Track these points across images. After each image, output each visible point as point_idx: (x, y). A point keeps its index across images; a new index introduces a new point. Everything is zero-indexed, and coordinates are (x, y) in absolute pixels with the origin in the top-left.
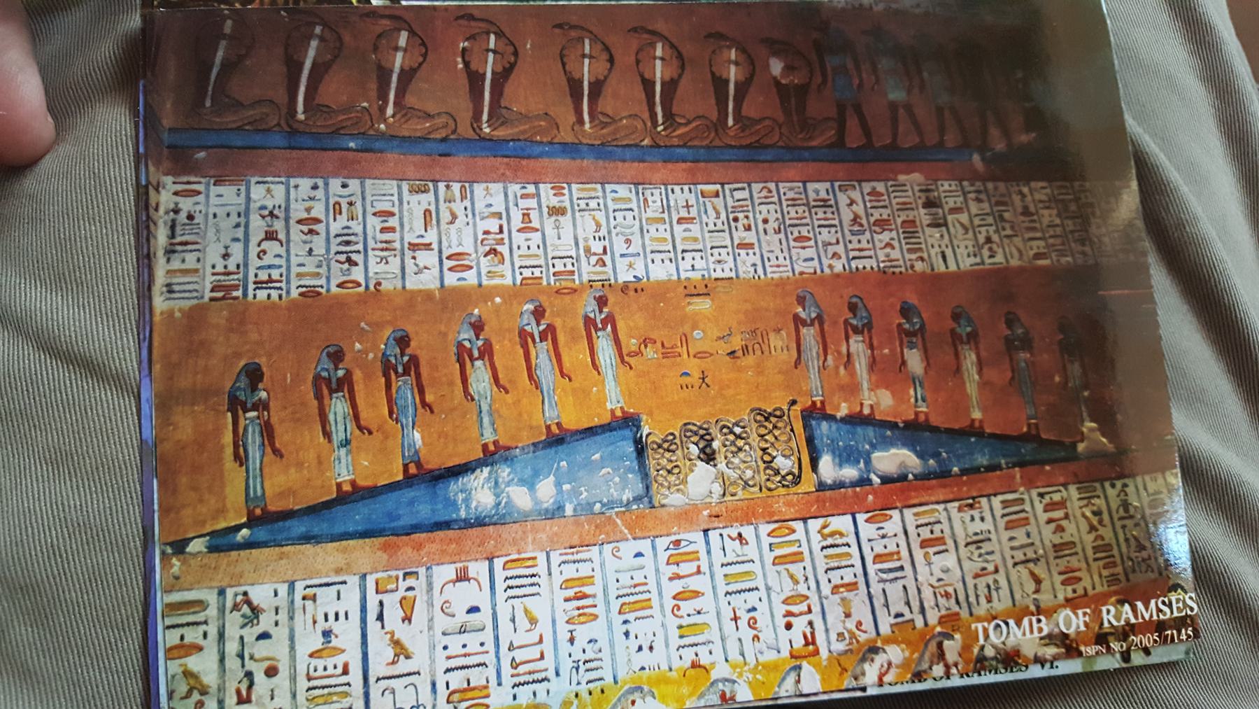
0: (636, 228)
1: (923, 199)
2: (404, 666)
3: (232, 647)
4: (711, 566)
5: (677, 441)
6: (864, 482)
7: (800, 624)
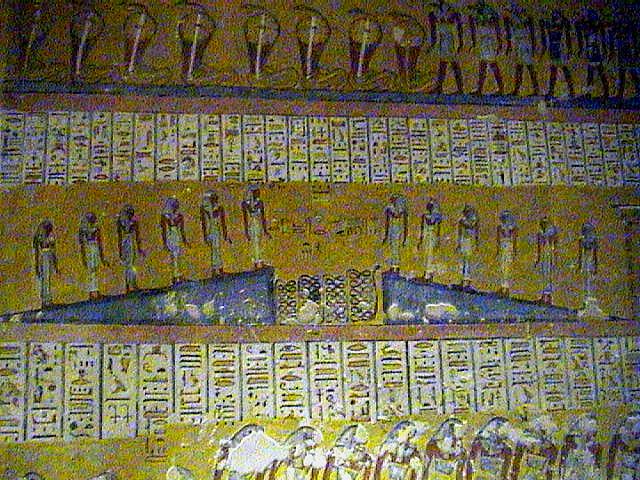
0: (284, 146)
1: (495, 134)
2: (122, 394)
3: (33, 373)
4: (308, 362)
5: (296, 286)
6: (417, 321)
7: (361, 402)
